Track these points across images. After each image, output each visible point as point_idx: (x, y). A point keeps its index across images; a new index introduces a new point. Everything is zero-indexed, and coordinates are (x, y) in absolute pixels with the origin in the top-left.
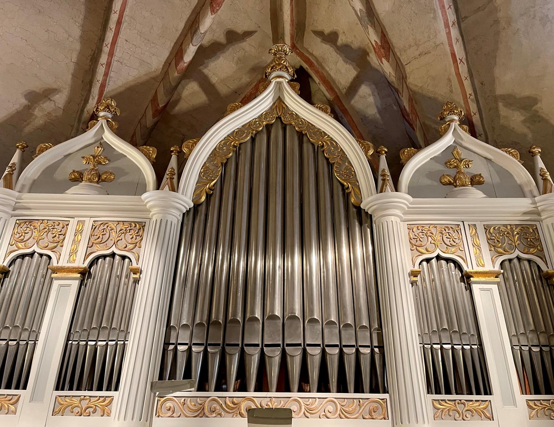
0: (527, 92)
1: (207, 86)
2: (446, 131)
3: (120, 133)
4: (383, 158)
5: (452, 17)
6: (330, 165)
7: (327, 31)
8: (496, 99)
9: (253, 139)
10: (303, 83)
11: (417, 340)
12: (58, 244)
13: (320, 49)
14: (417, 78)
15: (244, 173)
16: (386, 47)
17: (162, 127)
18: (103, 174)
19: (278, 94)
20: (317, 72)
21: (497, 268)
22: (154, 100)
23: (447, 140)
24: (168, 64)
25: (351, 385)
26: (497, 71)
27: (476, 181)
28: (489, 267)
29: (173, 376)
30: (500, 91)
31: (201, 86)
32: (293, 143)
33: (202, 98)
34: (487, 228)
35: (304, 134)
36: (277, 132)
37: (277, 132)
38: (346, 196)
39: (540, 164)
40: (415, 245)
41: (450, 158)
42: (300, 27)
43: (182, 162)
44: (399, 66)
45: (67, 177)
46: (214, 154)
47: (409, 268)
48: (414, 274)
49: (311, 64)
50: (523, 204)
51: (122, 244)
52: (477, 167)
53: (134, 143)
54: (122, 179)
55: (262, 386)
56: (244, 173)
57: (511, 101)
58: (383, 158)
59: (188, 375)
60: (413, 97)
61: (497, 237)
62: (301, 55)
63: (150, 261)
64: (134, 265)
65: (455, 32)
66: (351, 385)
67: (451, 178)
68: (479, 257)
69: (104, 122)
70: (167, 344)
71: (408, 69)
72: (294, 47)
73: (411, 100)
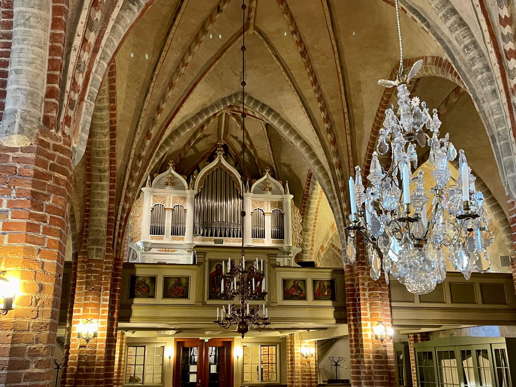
0: (289, 163)
1: (195, 150)
2: (265, 175)
3: (176, 171)
4: (248, 182)
5: (269, 144)
6: (234, 183)
7: (235, 136)
8: (281, 163)
9: (213, 173)
10: (227, 154)
11: (251, 228)
12: (164, 202)
13: (232, 140)
14: (260, 155)
15: (210, 183)
16: (252, 145)
17: (187, 167)
18: (173, 183)
19: (220, 159)
20: (231, 147)
21: (271, 212)
22: (180, 155)
23: (265, 177)
24: (185, 145)
25: (232, 235)
26: (281, 157)
27: (270, 189)
28: (269, 212)
29: (196, 233)
30: (282, 162)
31: (194, 150)
32: (223, 174)
33: (194, 153)
34: (271, 202)
35: (227, 172)
36: (219, 171)
37: (219, 171)
38: (237, 192)
39: (287, 185)
40: (253, 206)
41: (265, 182)
42: (226, 132)
43: (194, 180)
44: (255, 151)
45: (164, 184)
46: (202, 177)
47: (251, 211)
48: (252, 213)
49: (229, 144)
50: (280, 196)
51: (181, 203)
52: (271, 186)
53: (180, 174)
54: (179, 185)
55: (216, 236)
56: (210, 183)
57: (285, 165)
58: (248, 182)
59: (199, 233)
60: (259, 160)
61: (273, 204)
62: (226, 141)
63: (189, 207)
64: (184, 208)
65: (269, 147)
66: (232, 235)
67: (263, 189)
68: (268, 209)
69: (171, 167)
70: (194, 227)
71: (258, 152)
72: (224, 138)
73: (258, 161)
